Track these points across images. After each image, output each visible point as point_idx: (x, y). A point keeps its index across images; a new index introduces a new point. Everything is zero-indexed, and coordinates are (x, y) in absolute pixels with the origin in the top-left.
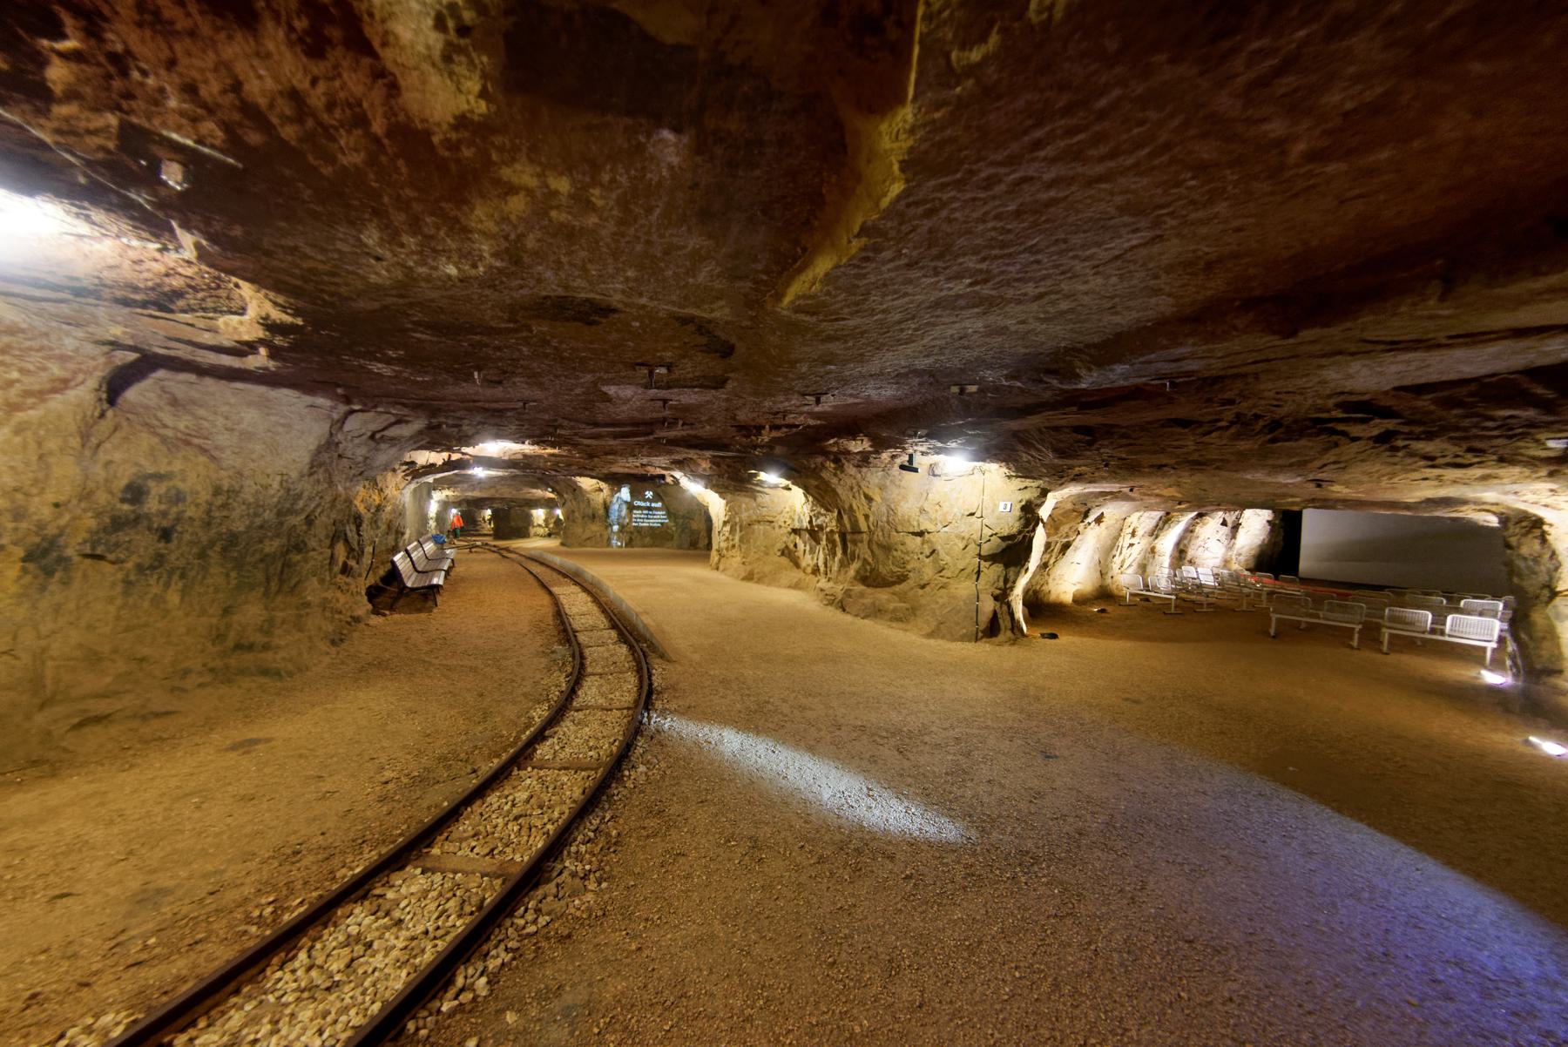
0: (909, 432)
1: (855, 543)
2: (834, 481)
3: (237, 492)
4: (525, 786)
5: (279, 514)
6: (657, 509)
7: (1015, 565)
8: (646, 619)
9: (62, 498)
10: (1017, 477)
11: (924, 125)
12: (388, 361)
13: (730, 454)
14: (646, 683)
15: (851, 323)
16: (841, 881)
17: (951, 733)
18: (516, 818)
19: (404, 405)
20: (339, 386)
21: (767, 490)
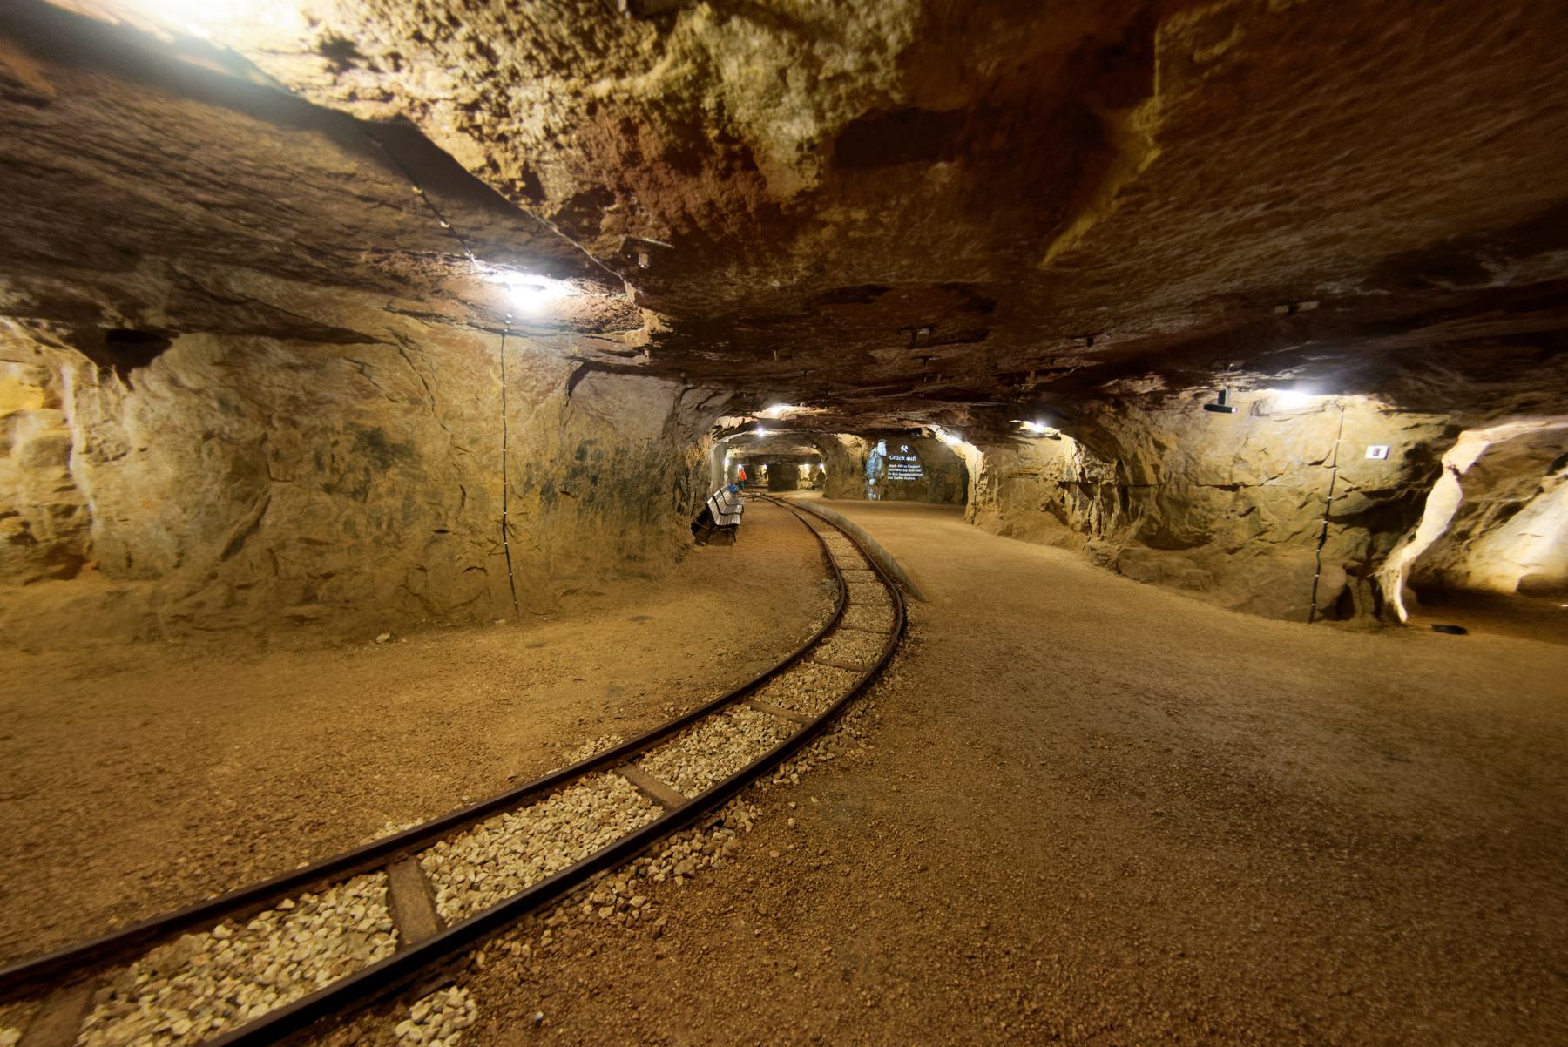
0: (1217, 365)
1: (1138, 498)
2: (1114, 427)
3: (625, 452)
4: (809, 673)
5: (647, 467)
6: (912, 463)
7: (1390, 529)
8: (902, 564)
9: (553, 457)
10: (1400, 411)
11: (1174, 106)
12: (717, 350)
13: (990, 404)
14: (901, 616)
15: (1121, 266)
16: (1082, 797)
17: (1245, 710)
18: (807, 691)
19: (719, 381)
20: (681, 371)
21: (1030, 441)
